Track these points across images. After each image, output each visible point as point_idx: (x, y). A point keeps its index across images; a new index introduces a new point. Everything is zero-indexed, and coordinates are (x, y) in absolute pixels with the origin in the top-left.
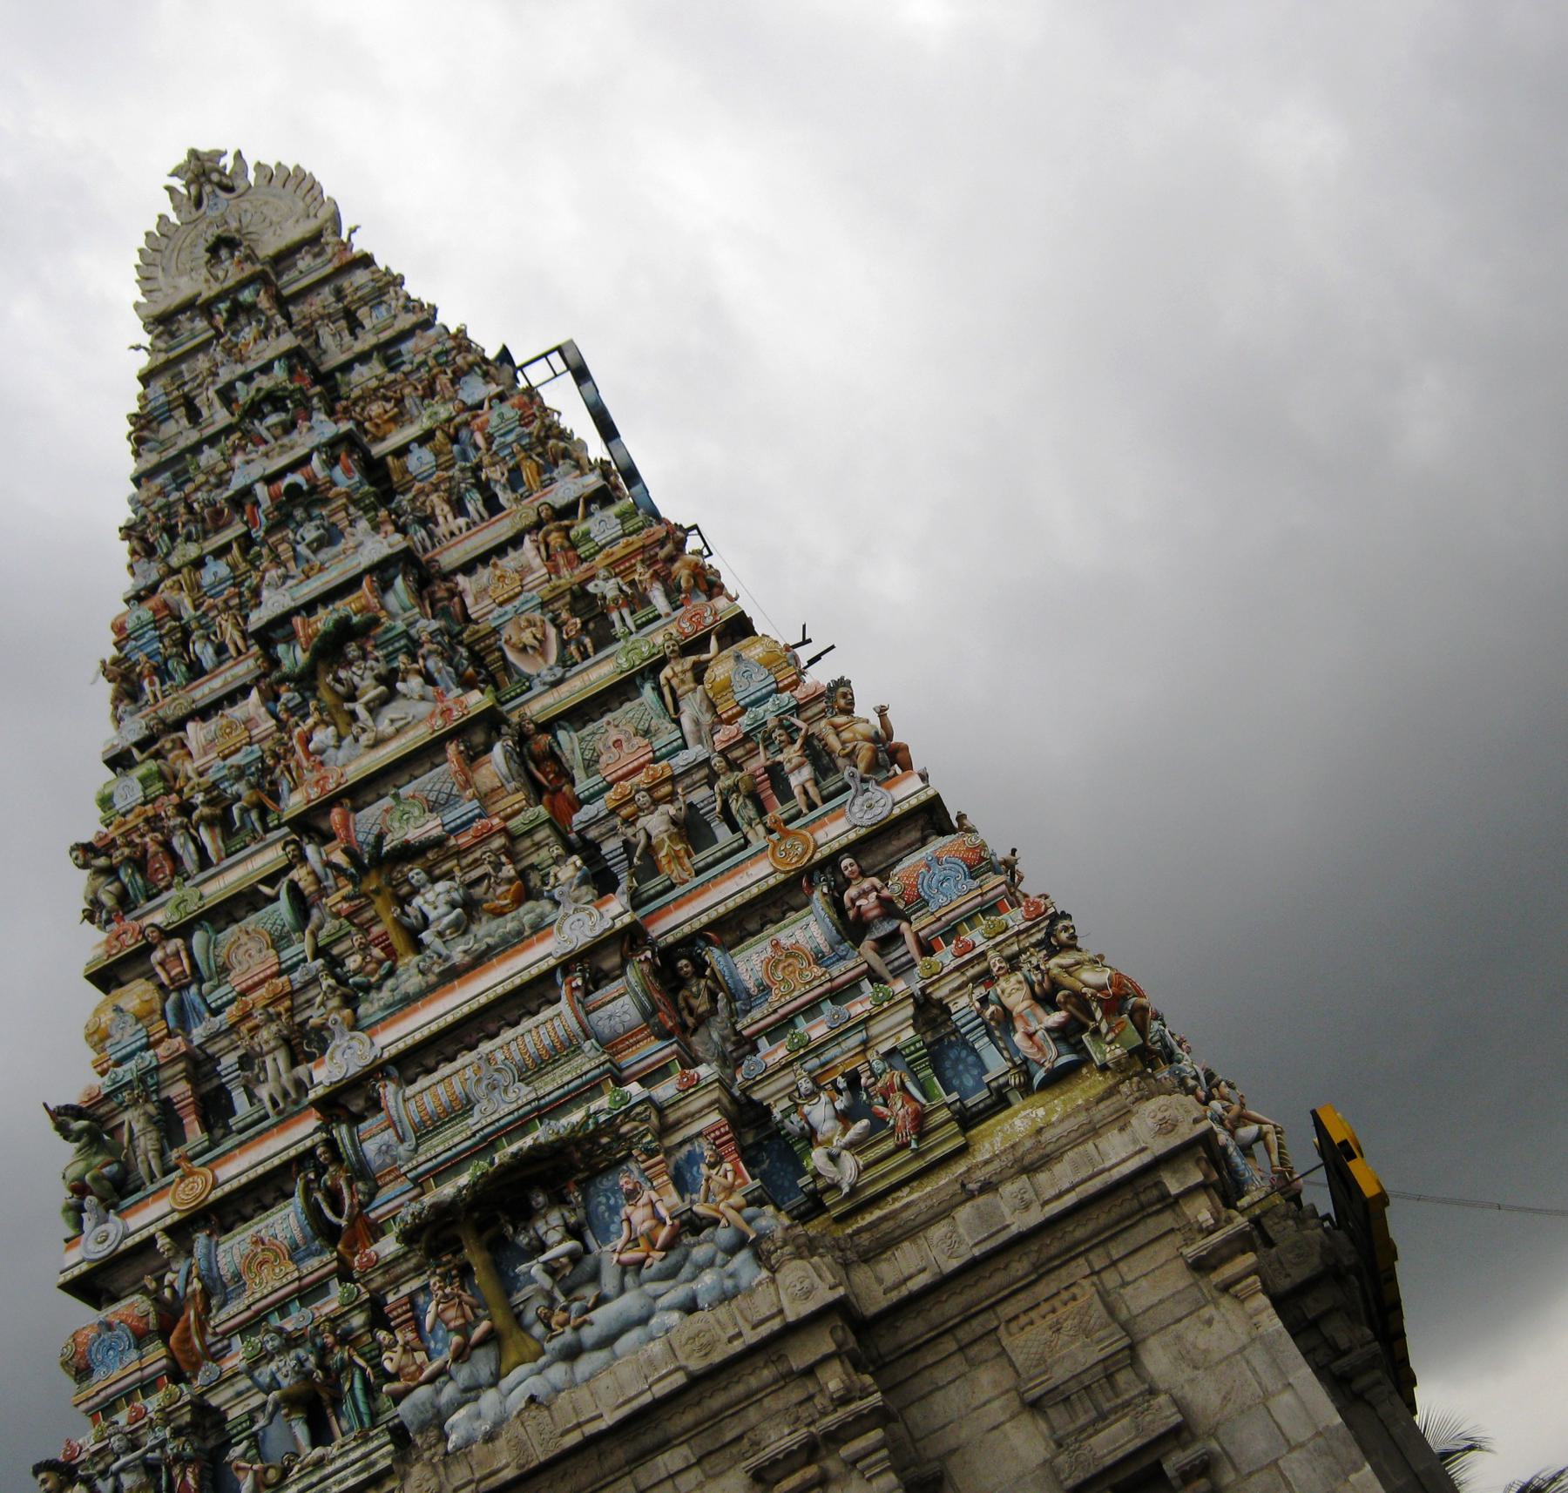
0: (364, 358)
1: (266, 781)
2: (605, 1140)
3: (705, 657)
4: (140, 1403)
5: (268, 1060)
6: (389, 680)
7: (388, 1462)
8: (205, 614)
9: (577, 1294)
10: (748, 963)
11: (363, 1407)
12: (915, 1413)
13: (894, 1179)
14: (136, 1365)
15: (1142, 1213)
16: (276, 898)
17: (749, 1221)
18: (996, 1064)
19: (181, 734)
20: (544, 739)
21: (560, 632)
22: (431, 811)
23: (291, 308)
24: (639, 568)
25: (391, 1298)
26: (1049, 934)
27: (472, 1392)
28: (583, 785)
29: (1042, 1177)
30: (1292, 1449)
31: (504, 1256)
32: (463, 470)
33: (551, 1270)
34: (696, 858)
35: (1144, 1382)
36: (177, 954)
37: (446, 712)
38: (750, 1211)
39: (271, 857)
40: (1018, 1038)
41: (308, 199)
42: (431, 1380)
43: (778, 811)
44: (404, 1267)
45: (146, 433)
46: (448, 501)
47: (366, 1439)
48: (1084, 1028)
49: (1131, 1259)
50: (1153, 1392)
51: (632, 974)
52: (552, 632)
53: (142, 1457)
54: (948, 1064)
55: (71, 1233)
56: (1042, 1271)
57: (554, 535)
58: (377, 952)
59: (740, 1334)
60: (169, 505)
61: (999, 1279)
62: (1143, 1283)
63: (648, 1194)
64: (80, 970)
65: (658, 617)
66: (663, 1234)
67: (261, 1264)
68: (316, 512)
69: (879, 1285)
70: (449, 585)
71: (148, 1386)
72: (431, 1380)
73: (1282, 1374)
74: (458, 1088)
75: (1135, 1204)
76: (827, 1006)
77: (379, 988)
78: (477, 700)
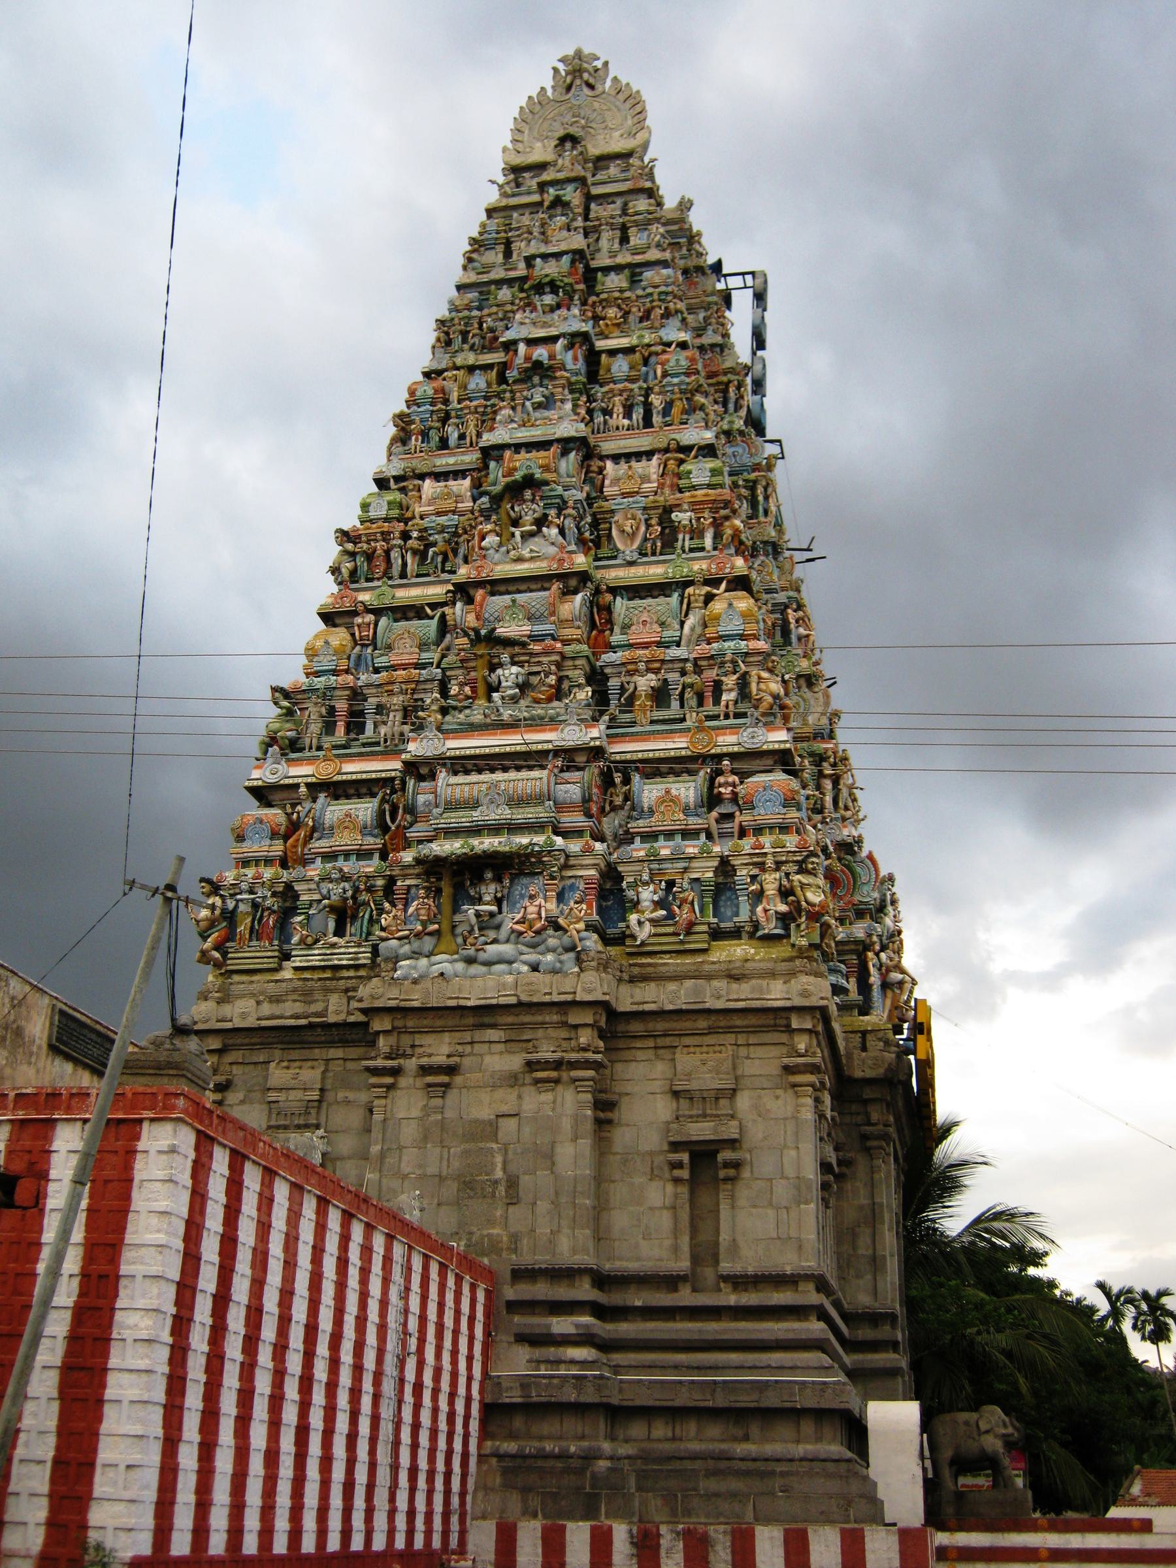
0: (618, 269)
1: (456, 543)
2: (533, 860)
3: (715, 591)
4: (261, 869)
5: (391, 715)
6: (541, 522)
7: (365, 961)
8: (461, 409)
9: (485, 932)
10: (649, 792)
11: (365, 929)
12: (619, 1067)
13: (665, 948)
14: (266, 848)
15: (774, 1028)
16: (432, 618)
17: (581, 940)
18: (744, 915)
19: (420, 482)
20: (608, 597)
21: (647, 529)
22: (529, 619)
23: (593, 206)
24: (707, 511)
25: (399, 883)
26: (804, 861)
27: (416, 955)
28: (616, 638)
29: (735, 986)
30: (782, 1177)
31: (461, 897)
32: (640, 388)
33: (478, 915)
34: (655, 713)
35: (732, 1109)
36: (369, 624)
37: (561, 561)
38: (584, 934)
39: (437, 592)
40: (759, 909)
41: (635, 120)
42: (399, 939)
43: (709, 708)
44: (411, 871)
45: (474, 256)
46: (624, 406)
47: (359, 945)
48: (794, 920)
49: (760, 1047)
50: (733, 1117)
51: (586, 774)
52: (643, 528)
53: (253, 900)
54: (723, 898)
55: (259, 755)
56: (711, 1031)
57: (672, 462)
58: (467, 689)
59: (550, 994)
60: (469, 318)
61: (688, 1024)
62: (757, 1062)
63: (540, 901)
64: (315, 608)
65: (703, 549)
66: (538, 925)
67: (346, 828)
68: (546, 382)
69: (627, 999)
70: (601, 464)
71: (268, 862)
72: (399, 939)
73: (797, 1141)
74: (475, 793)
75: (772, 1022)
76: (678, 838)
77: (460, 711)
78: (581, 561)
